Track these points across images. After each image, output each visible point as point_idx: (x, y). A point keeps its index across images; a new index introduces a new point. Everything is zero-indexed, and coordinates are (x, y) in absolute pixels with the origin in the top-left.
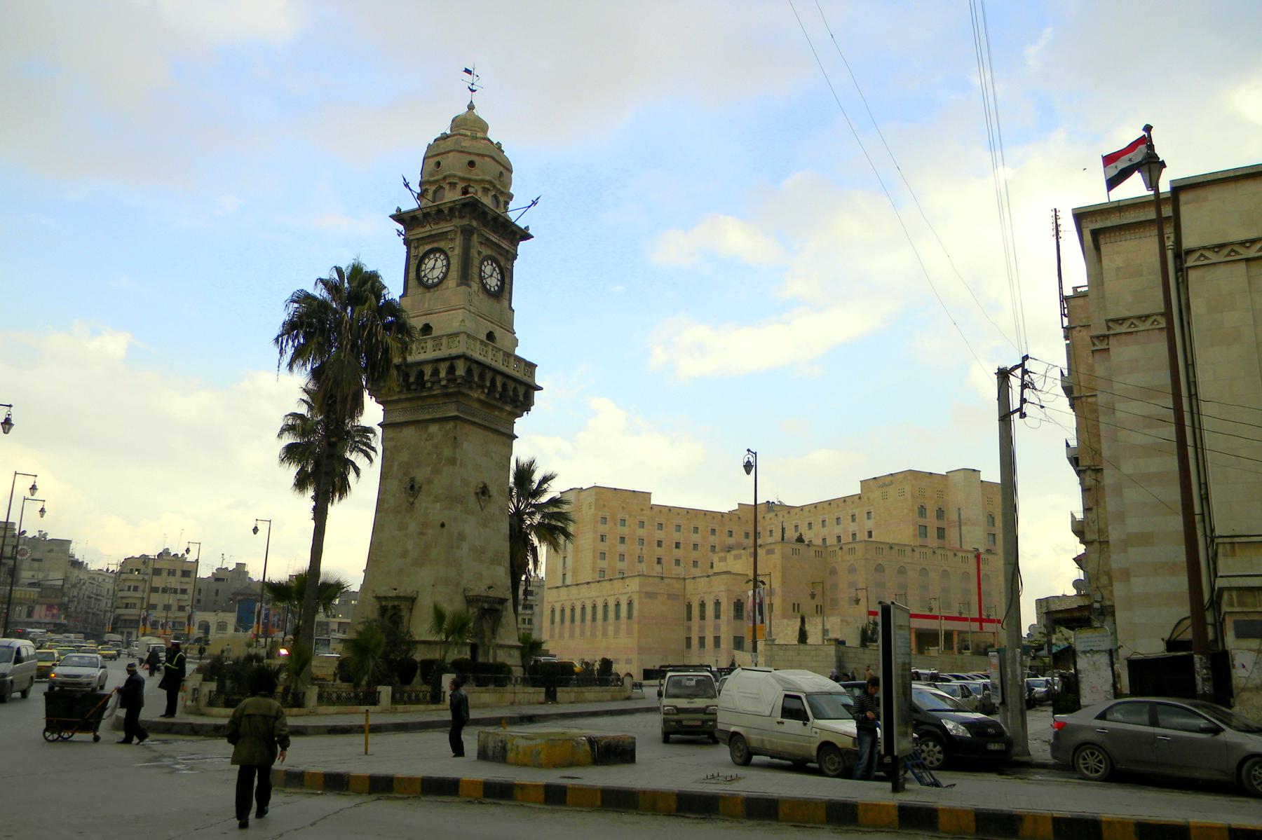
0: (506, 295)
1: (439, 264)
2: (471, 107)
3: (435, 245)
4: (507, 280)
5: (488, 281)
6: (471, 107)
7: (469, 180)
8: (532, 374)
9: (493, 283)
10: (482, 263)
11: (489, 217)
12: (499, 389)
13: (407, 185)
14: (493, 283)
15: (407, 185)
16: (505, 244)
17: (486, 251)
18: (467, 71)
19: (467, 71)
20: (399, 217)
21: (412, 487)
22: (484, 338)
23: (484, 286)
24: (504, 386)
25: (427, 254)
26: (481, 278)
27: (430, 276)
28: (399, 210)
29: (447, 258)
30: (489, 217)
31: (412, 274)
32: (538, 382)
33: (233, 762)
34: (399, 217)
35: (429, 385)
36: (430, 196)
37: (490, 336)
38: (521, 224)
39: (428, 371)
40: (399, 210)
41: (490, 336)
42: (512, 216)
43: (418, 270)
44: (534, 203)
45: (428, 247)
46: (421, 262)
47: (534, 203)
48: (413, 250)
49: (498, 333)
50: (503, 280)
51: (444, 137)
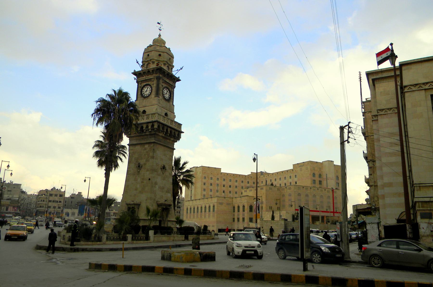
1: (149, 89)
2: (160, 36)
3: (147, 83)
4: (172, 95)
6: (160, 36)
10: (163, 89)
12: (169, 133)
13: (137, 62)
14: (167, 96)
15: (137, 62)
17: (165, 85)
18: (158, 23)
19: (158, 23)
20: (135, 73)
21: (139, 166)
23: (164, 97)
25: (144, 86)
26: (163, 95)
27: (145, 94)
28: (135, 71)
29: (151, 88)
31: (139, 93)
32: (182, 130)
34: (135, 73)
35: (145, 131)
37: (166, 114)
38: (177, 76)
39: (145, 126)
40: (135, 71)
41: (166, 114)
42: (174, 73)
43: (141, 92)
44: (181, 69)
47: (181, 69)
48: (139, 85)
49: (169, 113)
50: (170, 95)
51: (150, 46)
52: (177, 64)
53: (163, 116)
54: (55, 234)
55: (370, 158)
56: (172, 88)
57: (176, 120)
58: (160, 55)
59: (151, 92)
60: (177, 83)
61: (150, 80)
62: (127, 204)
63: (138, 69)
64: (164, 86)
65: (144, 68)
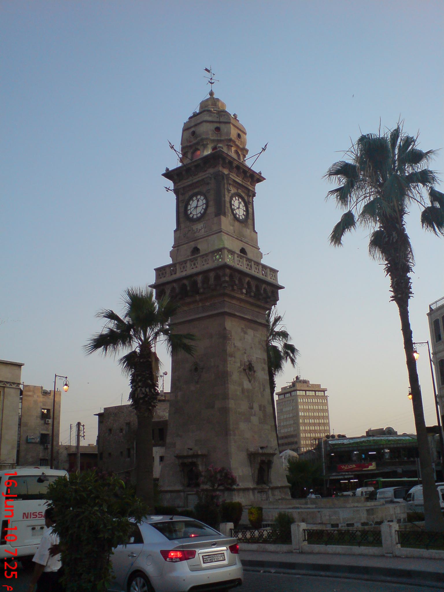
0: (250, 221)
1: (201, 203)
2: (211, 94)
3: (196, 190)
4: (250, 210)
5: (237, 211)
6: (211, 94)
7: (220, 122)
8: (276, 277)
9: (241, 213)
10: (231, 199)
11: (234, 165)
12: (254, 289)
13: (172, 147)
14: (241, 213)
15: (172, 147)
16: (248, 185)
17: (233, 190)
18: (206, 70)
19: (206, 70)
20: (168, 175)
21: (196, 369)
22: (238, 252)
23: (234, 215)
24: (257, 287)
25: (191, 198)
26: (233, 210)
27: (194, 213)
28: (167, 169)
29: (206, 198)
30: (234, 165)
31: (182, 215)
32: (280, 283)
33: (105, 409)
34: (168, 175)
35: (201, 290)
36: (189, 156)
37: (243, 251)
38: (256, 169)
39: (199, 279)
40: (167, 169)
41: (243, 251)
42: (248, 163)
43: (186, 210)
44: (264, 150)
45: (190, 193)
46: (187, 204)
47: (264, 150)
48: (180, 196)
49: (248, 249)
50: (247, 211)
51: (195, 115)
52: (252, 144)
53: (239, 256)
54: (305, 497)
55: (350, 444)
56: (249, 196)
57: (263, 261)
58: (218, 129)
59: (207, 207)
60: (257, 185)
61: (203, 182)
62: (178, 457)
63: (175, 163)
64: (232, 192)
65: (187, 161)
